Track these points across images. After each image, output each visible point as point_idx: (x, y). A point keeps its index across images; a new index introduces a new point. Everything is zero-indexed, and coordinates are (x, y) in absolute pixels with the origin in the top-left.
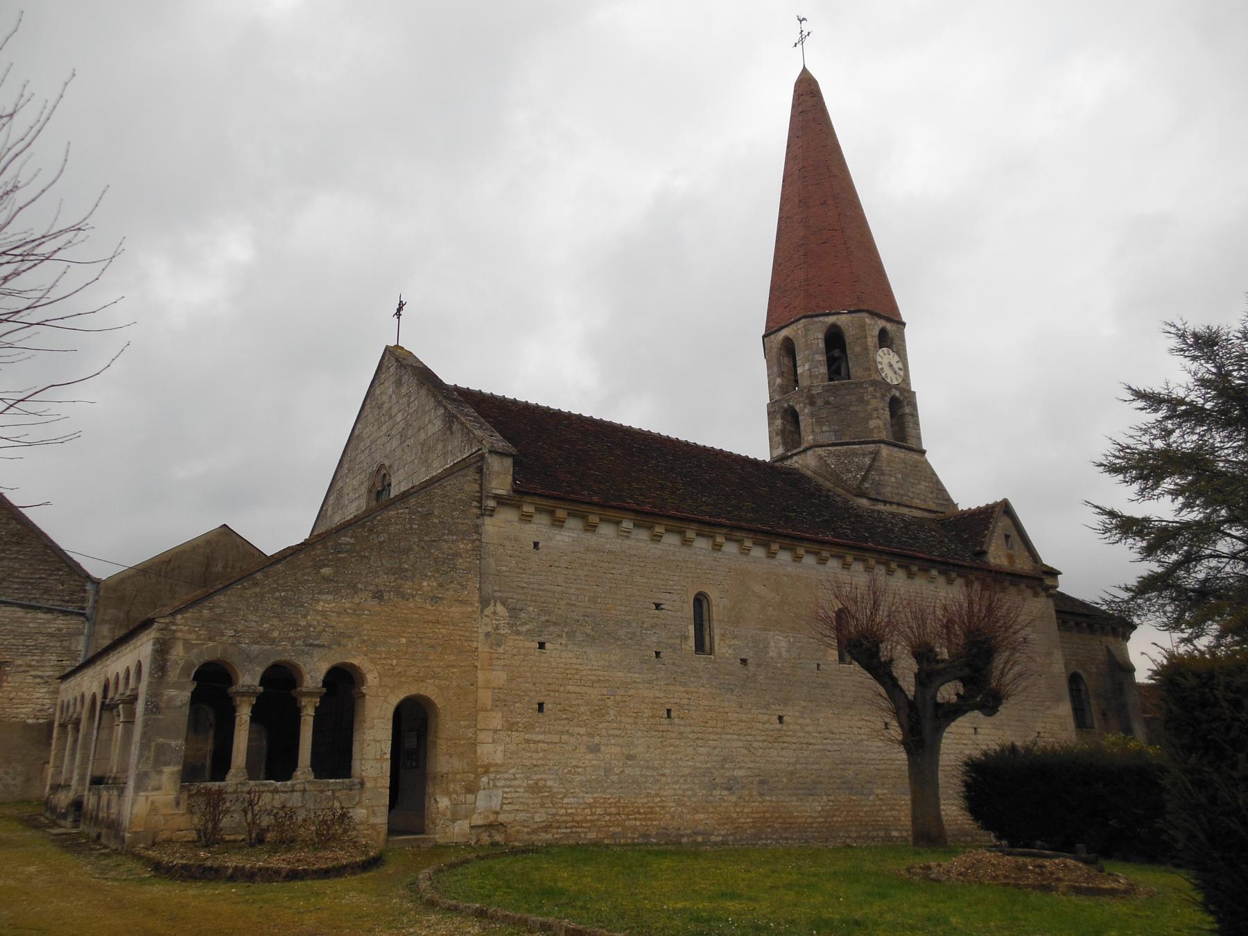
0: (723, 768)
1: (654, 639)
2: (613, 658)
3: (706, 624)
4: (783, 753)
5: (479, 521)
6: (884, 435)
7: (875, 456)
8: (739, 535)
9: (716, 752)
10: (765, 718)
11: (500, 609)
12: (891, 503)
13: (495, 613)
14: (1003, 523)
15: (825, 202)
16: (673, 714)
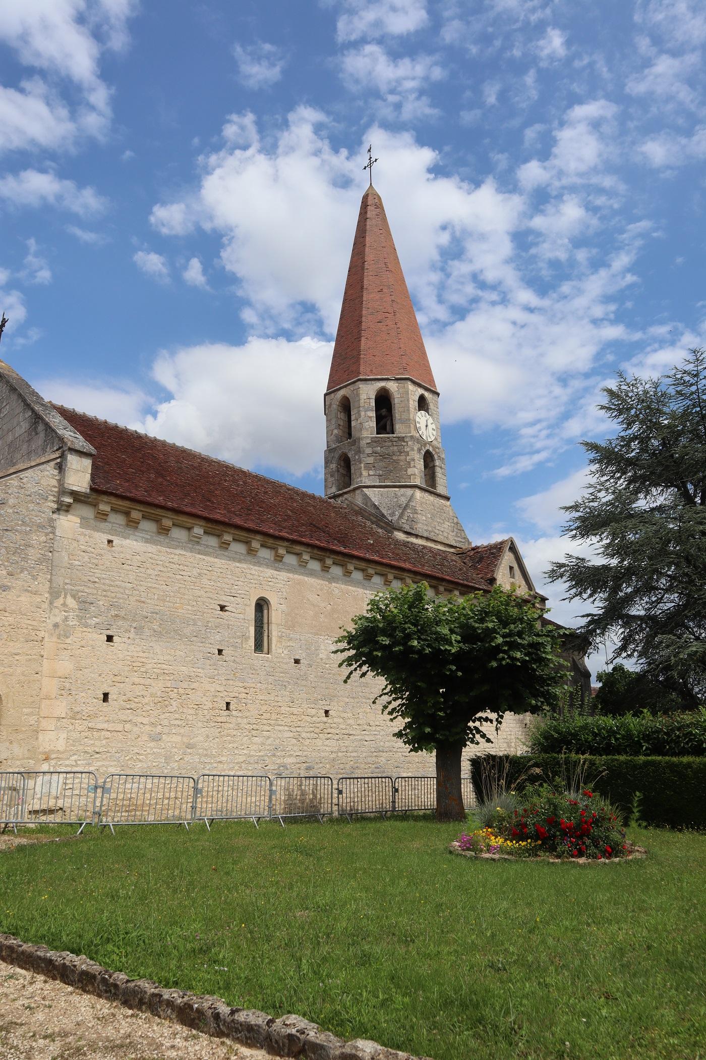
0: (274, 755)
1: (218, 637)
2: (178, 653)
3: (265, 626)
4: (327, 742)
5: (55, 516)
8: (298, 548)
9: (269, 741)
10: (313, 712)
11: (70, 602)
12: (422, 537)
13: (64, 605)
14: (507, 558)
15: (381, 291)
16: (231, 707)
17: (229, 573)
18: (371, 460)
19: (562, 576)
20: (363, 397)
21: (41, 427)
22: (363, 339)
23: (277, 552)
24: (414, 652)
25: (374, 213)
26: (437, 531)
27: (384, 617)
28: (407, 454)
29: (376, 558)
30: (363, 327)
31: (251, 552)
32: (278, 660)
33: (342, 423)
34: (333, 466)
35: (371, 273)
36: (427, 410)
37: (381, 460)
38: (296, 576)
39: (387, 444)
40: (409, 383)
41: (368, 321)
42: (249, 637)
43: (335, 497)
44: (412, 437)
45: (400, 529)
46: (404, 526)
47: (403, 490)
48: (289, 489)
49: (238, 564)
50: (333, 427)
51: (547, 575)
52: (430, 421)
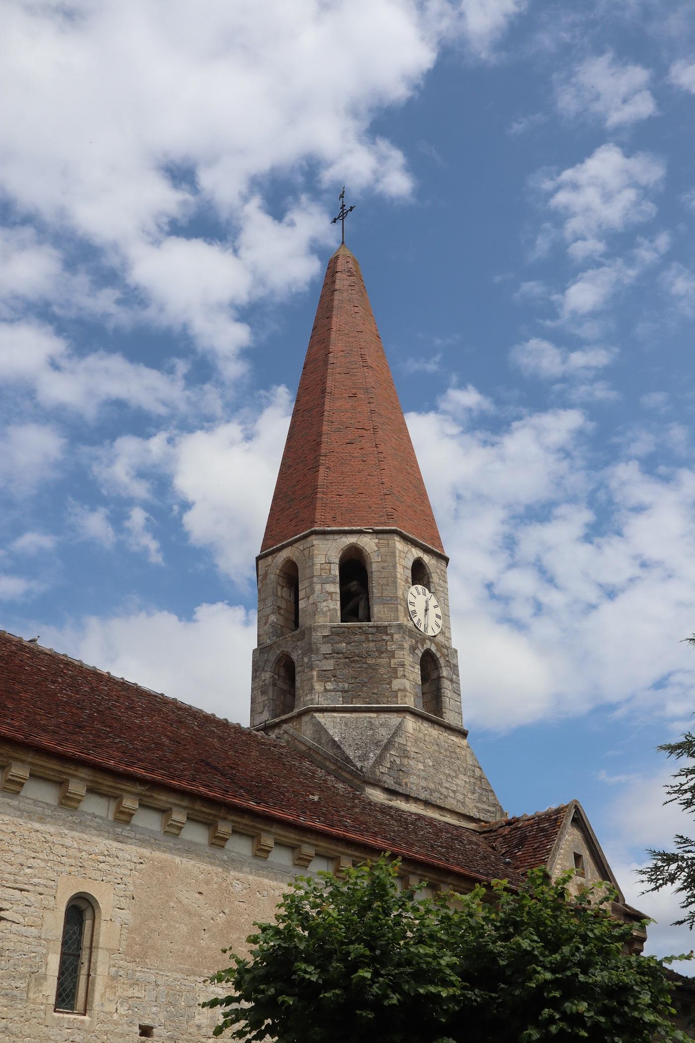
3: (85, 954)
6: (410, 702)
7: (398, 730)
8: (163, 799)
12: (417, 800)
17: (16, 841)
18: (329, 665)
19: (672, 878)
20: (319, 559)
22: (322, 469)
23: (120, 804)
24: (365, 1005)
25: (346, 283)
26: (444, 791)
27: (313, 931)
28: (392, 655)
29: (318, 825)
30: (323, 451)
31: (68, 802)
32: (105, 1027)
33: (283, 605)
34: (267, 676)
35: (338, 370)
36: (427, 585)
37: (346, 665)
38: (157, 854)
39: (357, 638)
40: (397, 538)
41: (331, 440)
42: (45, 977)
43: (267, 728)
44: (400, 626)
45: (376, 784)
46: (385, 778)
47: (383, 716)
48: (180, 709)
49: (37, 826)
50: (268, 610)
51: (645, 877)
52: (433, 602)
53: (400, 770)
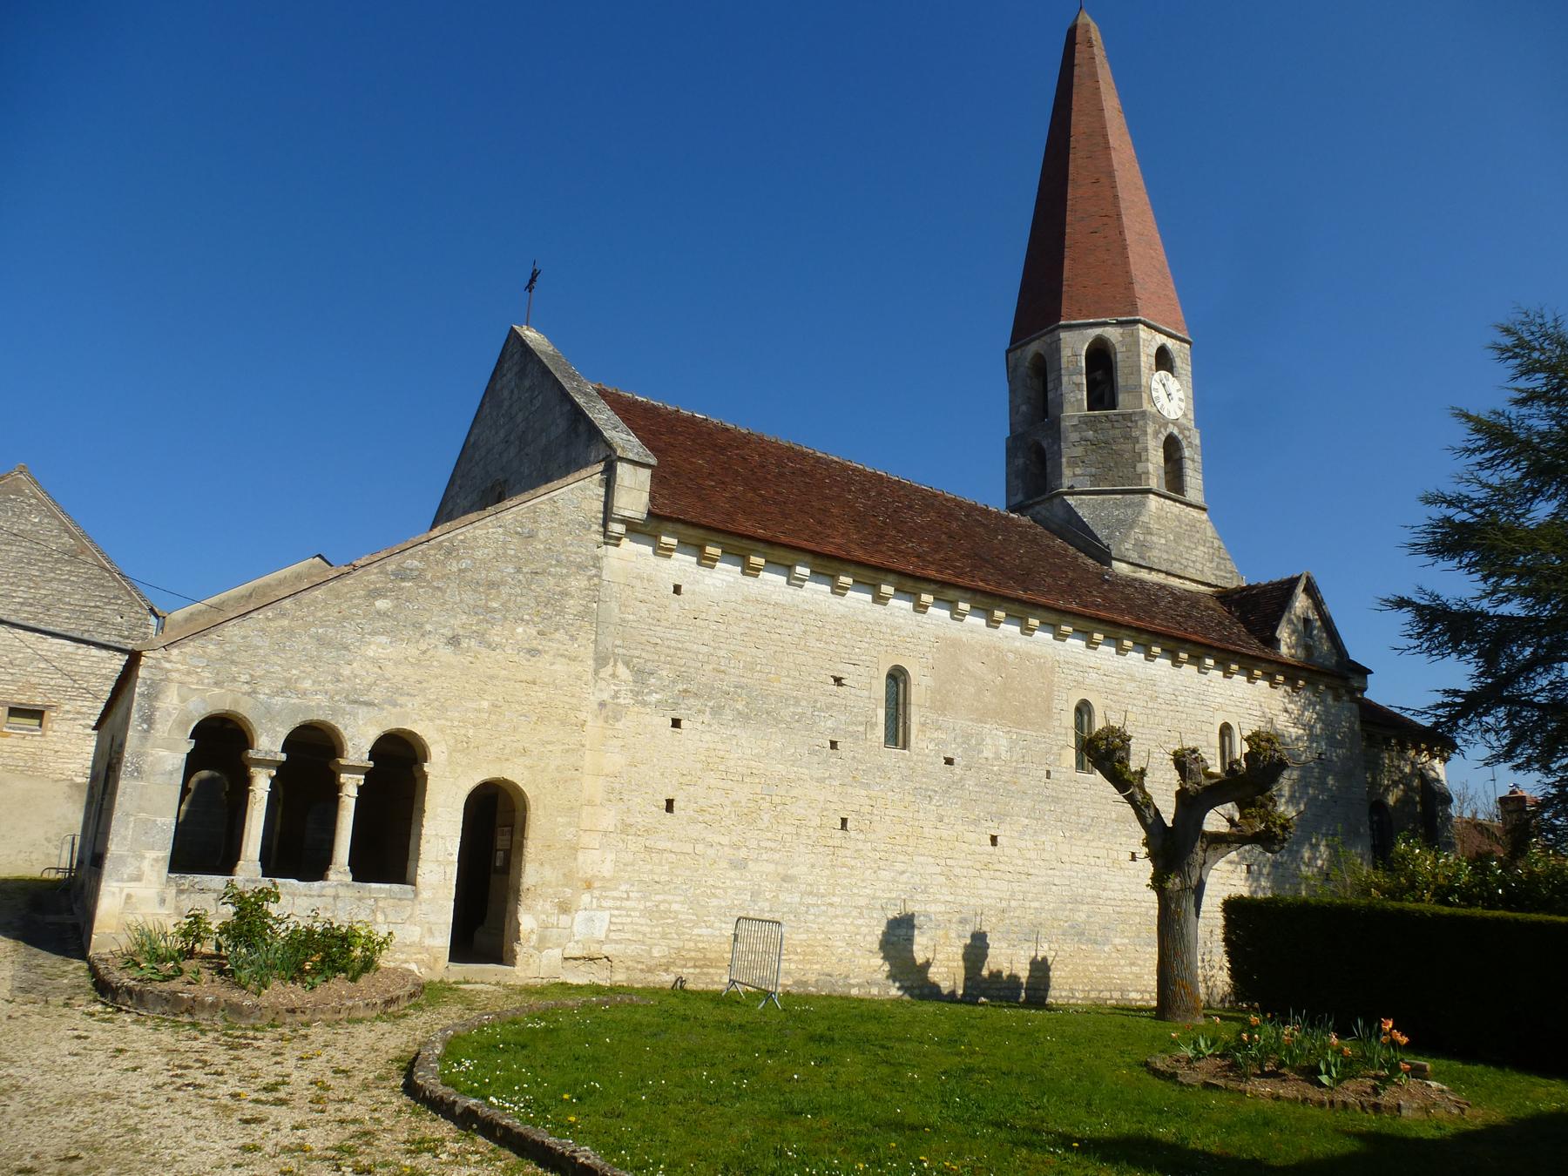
8: (951, 594)
11: (623, 671)
18: (1078, 451)
20: (1066, 353)
21: (582, 428)
53: (1141, 546)
